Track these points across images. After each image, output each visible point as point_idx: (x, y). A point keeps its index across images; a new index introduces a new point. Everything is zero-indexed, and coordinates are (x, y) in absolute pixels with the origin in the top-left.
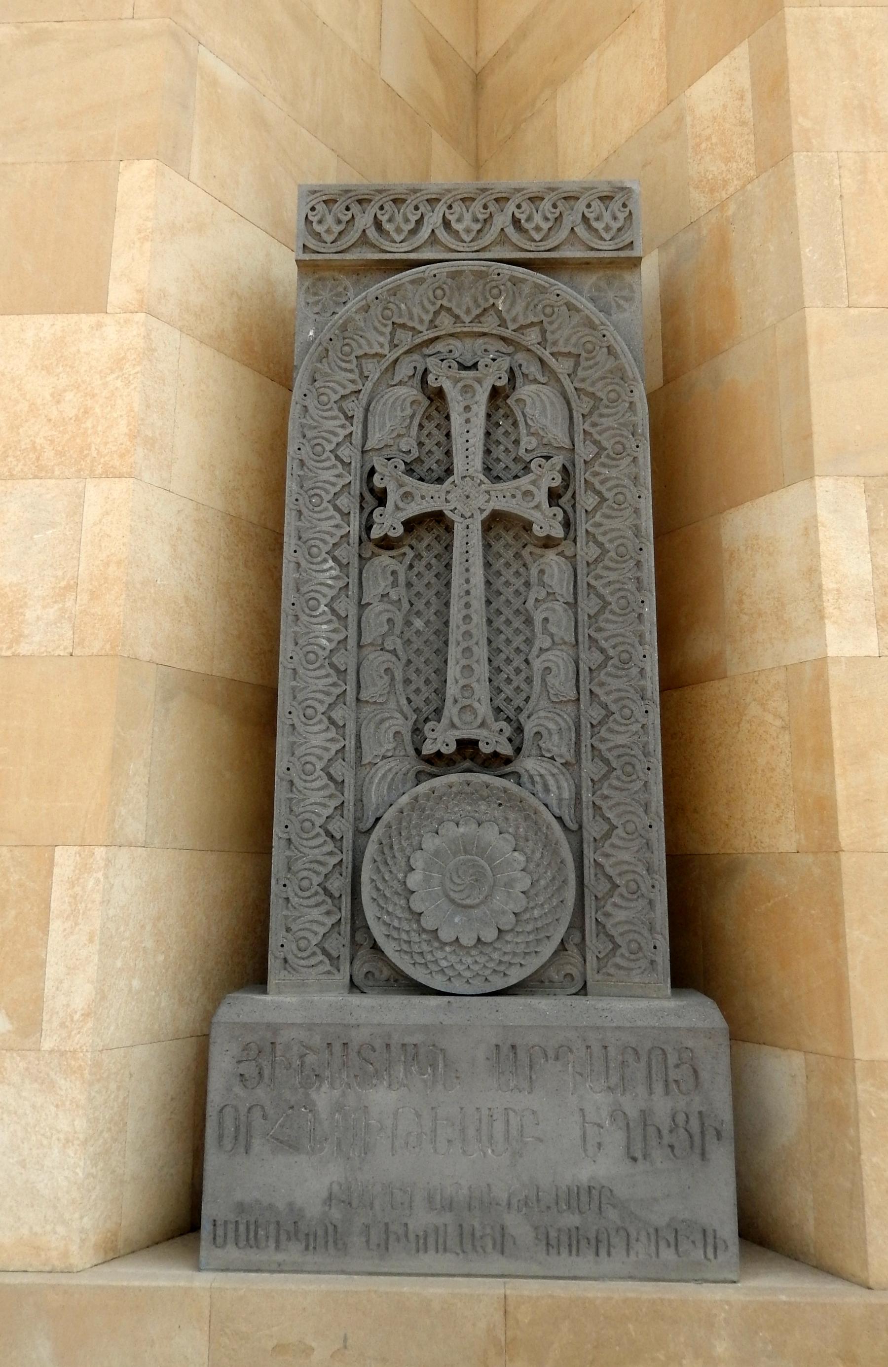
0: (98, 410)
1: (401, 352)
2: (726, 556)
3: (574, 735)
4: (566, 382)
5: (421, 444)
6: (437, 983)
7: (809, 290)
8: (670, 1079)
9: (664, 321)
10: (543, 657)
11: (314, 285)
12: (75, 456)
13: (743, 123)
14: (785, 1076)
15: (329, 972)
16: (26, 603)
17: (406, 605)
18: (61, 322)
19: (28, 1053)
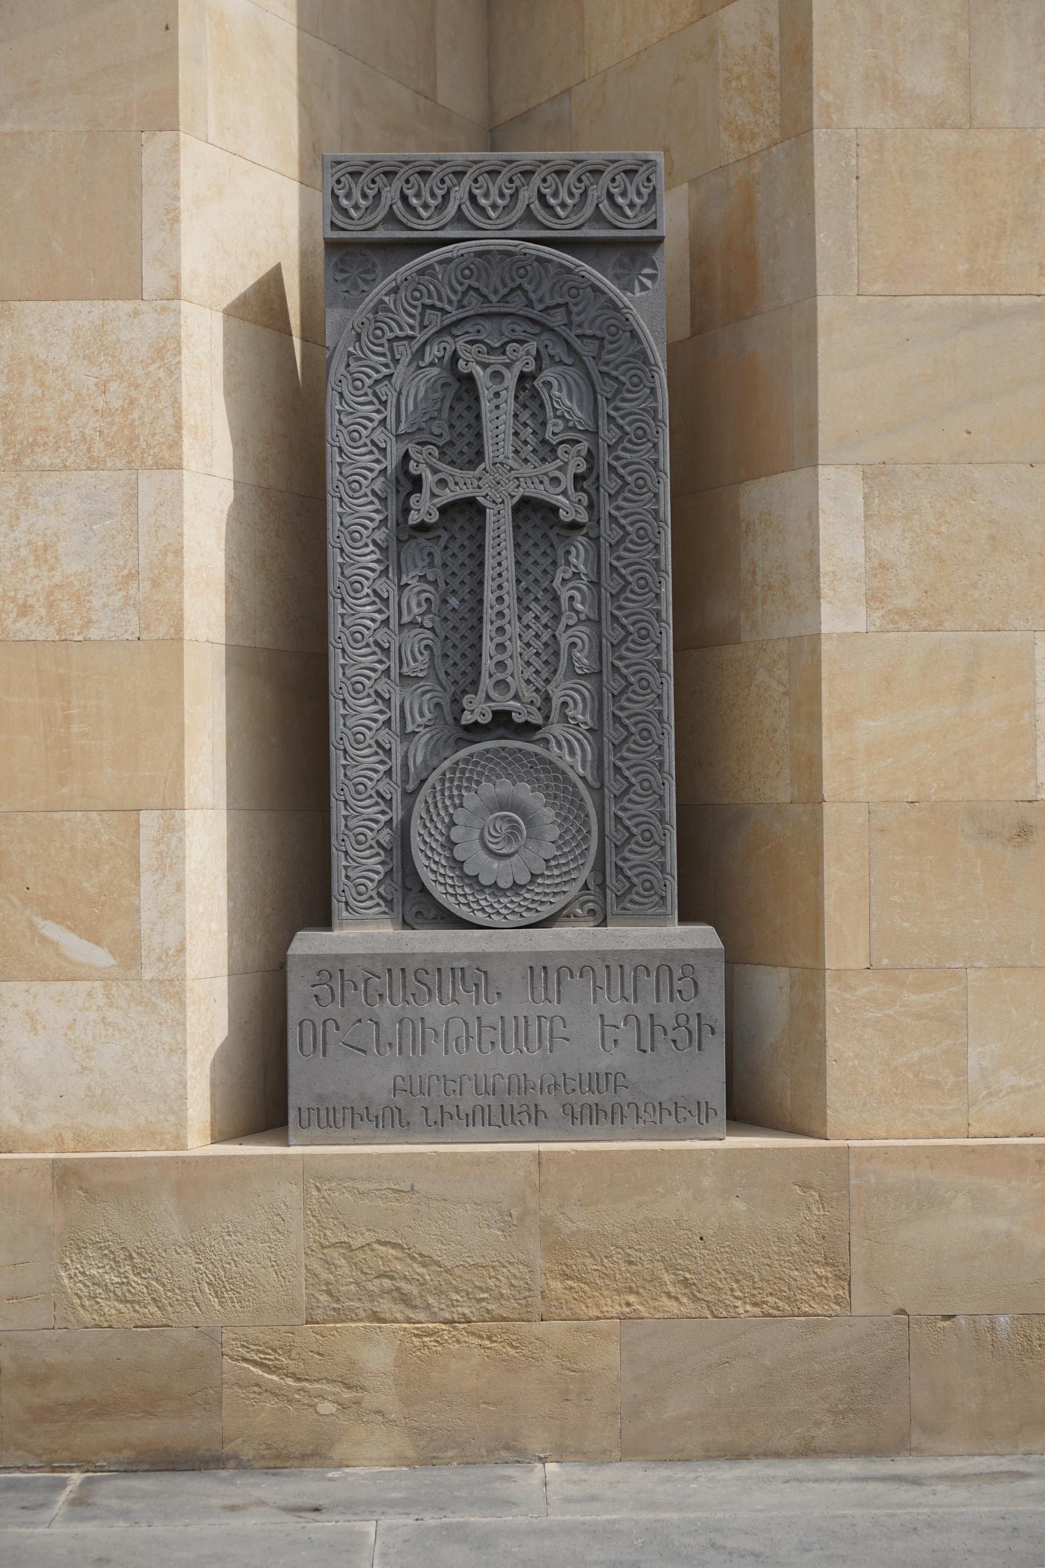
0: (142, 401)
1: (430, 333)
2: (743, 526)
3: (596, 704)
4: (590, 363)
5: (452, 426)
6: (479, 918)
7: (822, 277)
8: (675, 990)
9: (693, 265)
10: (570, 632)
11: (342, 260)
12: (125, 447)
13: (771, 76)
14: (772, 987)
15: (384, 913)
16: (91, 591)
17: (442, 586)
18: (98, 309)
19: (131, 982)
